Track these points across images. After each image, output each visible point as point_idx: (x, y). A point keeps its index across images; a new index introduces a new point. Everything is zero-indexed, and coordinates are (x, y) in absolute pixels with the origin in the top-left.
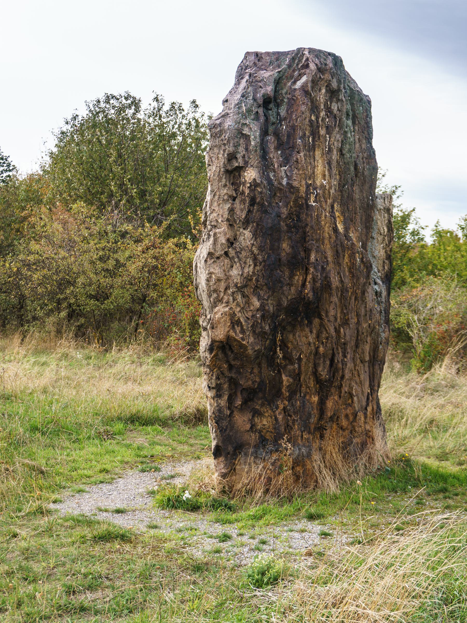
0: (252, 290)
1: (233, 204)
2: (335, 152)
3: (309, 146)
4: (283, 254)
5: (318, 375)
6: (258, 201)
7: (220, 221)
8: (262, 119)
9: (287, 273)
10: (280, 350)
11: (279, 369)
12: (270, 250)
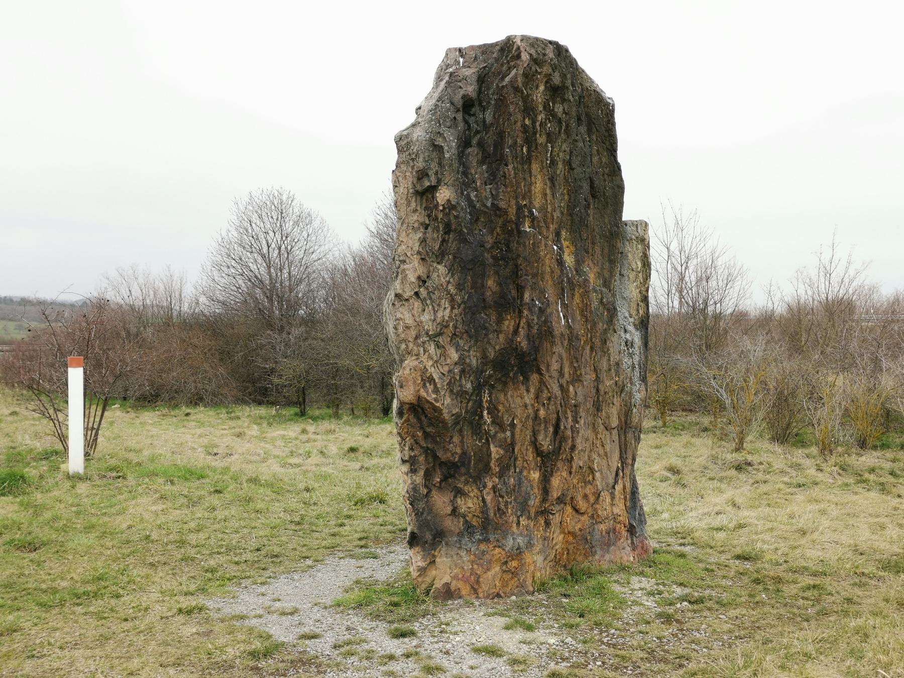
0: (449, 339)
1: (425, 233)
2: (560, 165)
3: (522, 158)
4: (489, 293)
5: (538, 446)
6: (453, 227)
7: (409, 254)
8: (461, 126)
9: (493, 318)
10: (488, 413)
11: (488, 438)
12: (472, 288)
